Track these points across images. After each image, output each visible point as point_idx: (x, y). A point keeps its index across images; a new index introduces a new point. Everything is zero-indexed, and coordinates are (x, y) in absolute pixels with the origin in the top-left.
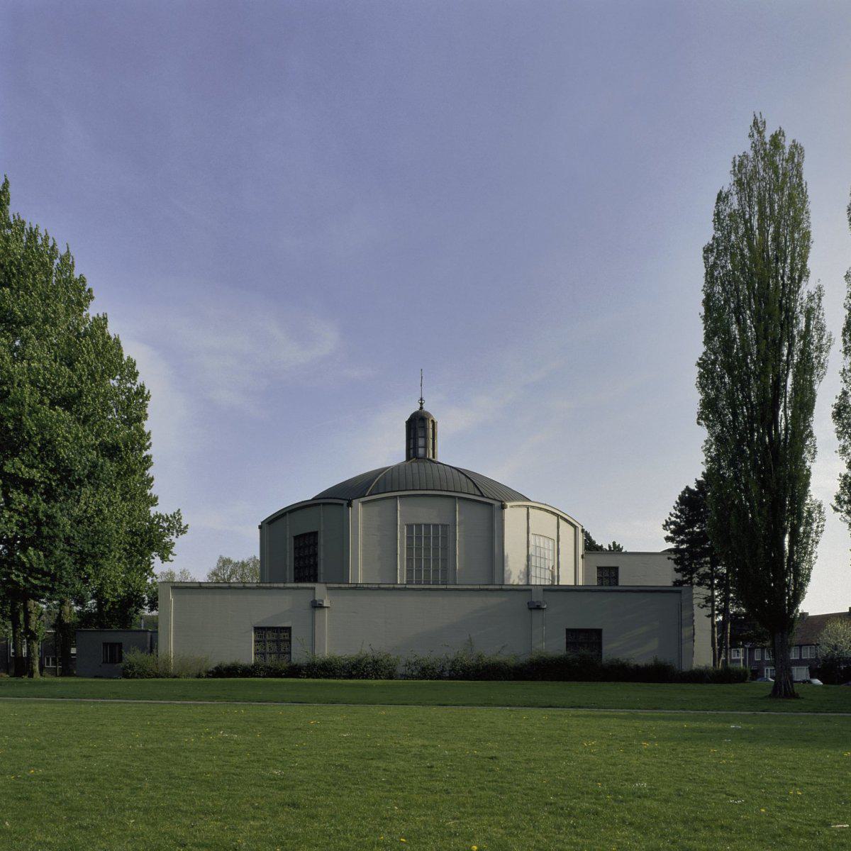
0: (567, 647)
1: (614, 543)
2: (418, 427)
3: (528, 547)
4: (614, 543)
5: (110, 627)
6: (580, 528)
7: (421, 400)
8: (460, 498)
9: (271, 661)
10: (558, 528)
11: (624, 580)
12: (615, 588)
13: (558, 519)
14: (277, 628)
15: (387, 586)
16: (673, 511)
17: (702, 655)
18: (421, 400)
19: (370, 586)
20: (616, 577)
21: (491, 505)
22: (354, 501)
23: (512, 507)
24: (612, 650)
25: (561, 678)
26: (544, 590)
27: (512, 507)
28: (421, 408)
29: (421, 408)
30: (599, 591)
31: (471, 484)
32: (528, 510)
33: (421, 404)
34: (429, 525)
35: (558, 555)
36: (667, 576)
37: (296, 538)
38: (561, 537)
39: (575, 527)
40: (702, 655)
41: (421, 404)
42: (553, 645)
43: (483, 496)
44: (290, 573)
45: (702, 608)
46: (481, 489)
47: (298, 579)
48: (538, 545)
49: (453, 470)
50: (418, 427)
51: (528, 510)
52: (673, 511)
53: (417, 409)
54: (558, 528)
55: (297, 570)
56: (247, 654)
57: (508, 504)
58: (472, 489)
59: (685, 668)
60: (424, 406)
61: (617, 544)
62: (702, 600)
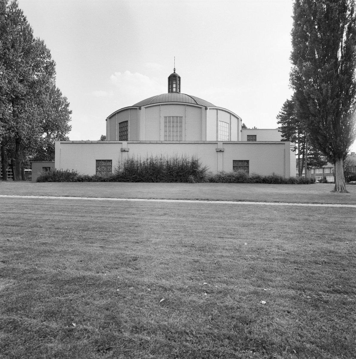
0: (233, 168)
1: (255, 127)
2: (174, 79)
3: (217, 126)
4: (255, 127)
5: (52, 161)
6: (240, 119)
7: (175, 69)
8: (162, 105)
9: (103, 175)
10: (230, 119)
11: (258, 139)
12: (255, 142)
13: (230, 116)
14: (106, 160)
15: (154, 142)
16: (281, 111)
17: (294, 172)
18: (175, 69)
19: (146, 142)
20: (256, 138)
21: (201, 108)
22: (142, 107)
23: (210, 109)
24: (254, 170)
25: (230, 182)
26: (223, 143)
27: (210, 109)
28: (174, 72)
29: (174, 72)
30: (248, 144)
31: (193, 101)
32: (217, 112)
33: (174, 71)
34: (170, 117)
35: (230, 130)
36: (278, 137)
37: (120, 124)
38: (232, 122)
39: (238, 119)
40: (294, 172)
41: (174, 71)
42: (229, 169)
43: (197, 104)
44: (117, 138)
45: (293, 151)
46: (197, 102)
47: (121, 140)
48: (223, 126)
49: (189, 97)
50: (174, 79)
51: (217, 112)
52: (281, 111)
53: (173, 72)
54: (230, 119)
55: (120, 137)
56: (91, 171)
57: (208, 108)
58: (193, 102)
59: (287, 177)
60: (175, 71)
61: (256, 128)
62: (294, 148)
